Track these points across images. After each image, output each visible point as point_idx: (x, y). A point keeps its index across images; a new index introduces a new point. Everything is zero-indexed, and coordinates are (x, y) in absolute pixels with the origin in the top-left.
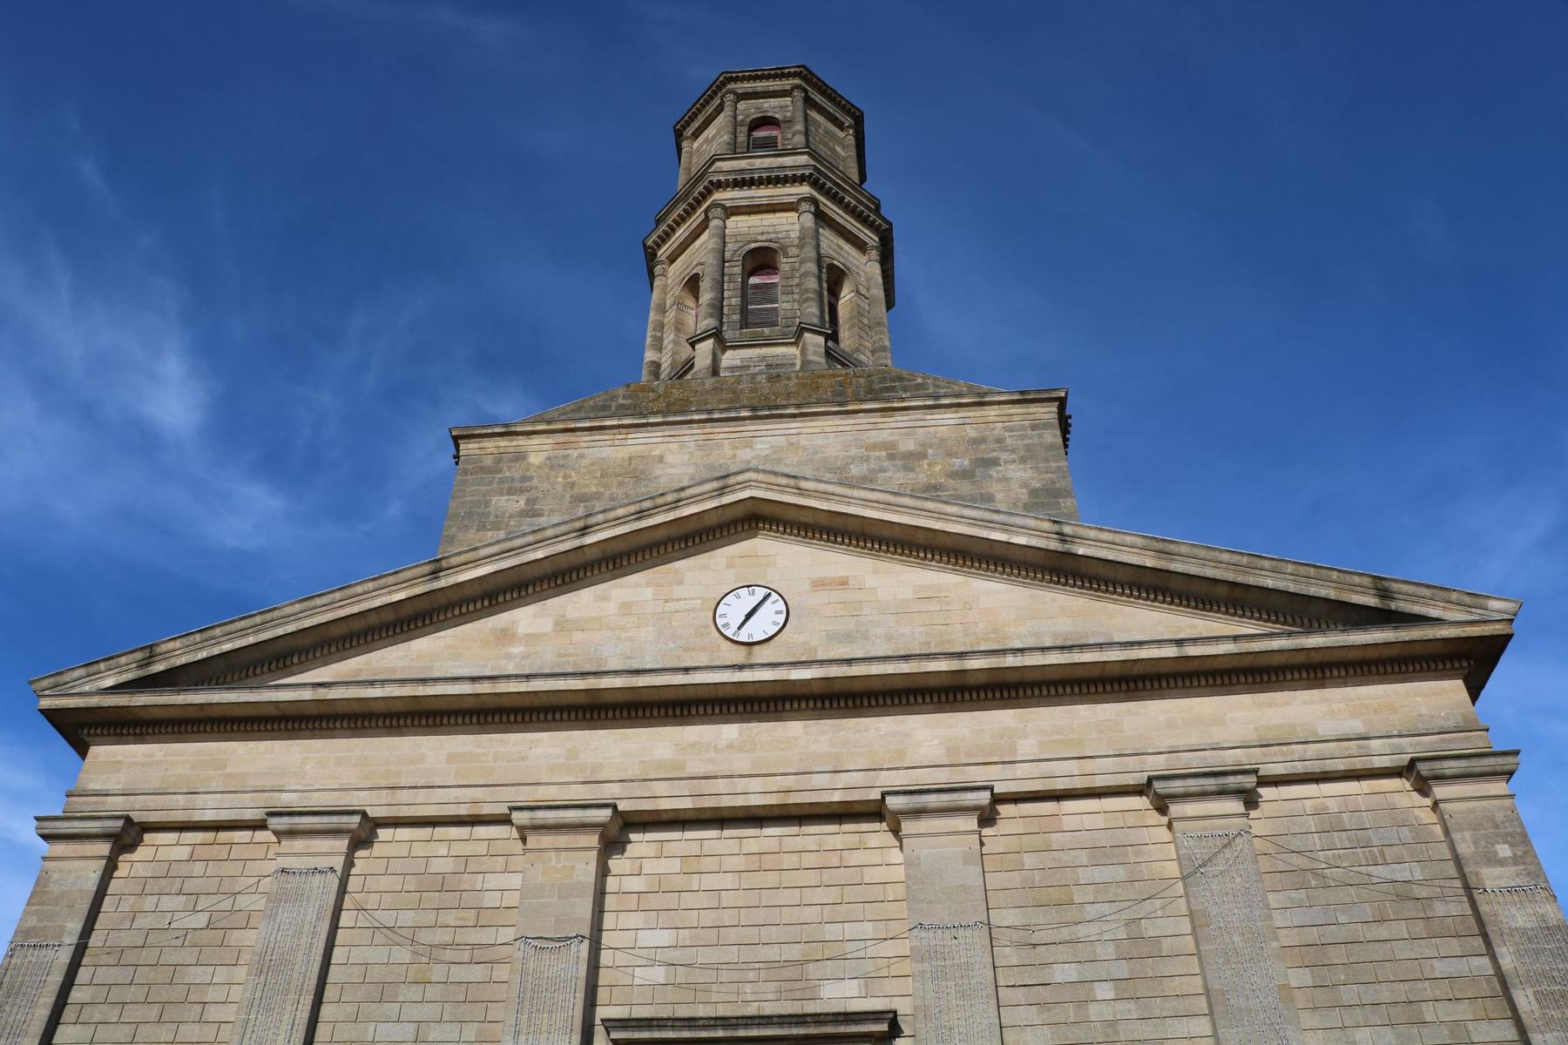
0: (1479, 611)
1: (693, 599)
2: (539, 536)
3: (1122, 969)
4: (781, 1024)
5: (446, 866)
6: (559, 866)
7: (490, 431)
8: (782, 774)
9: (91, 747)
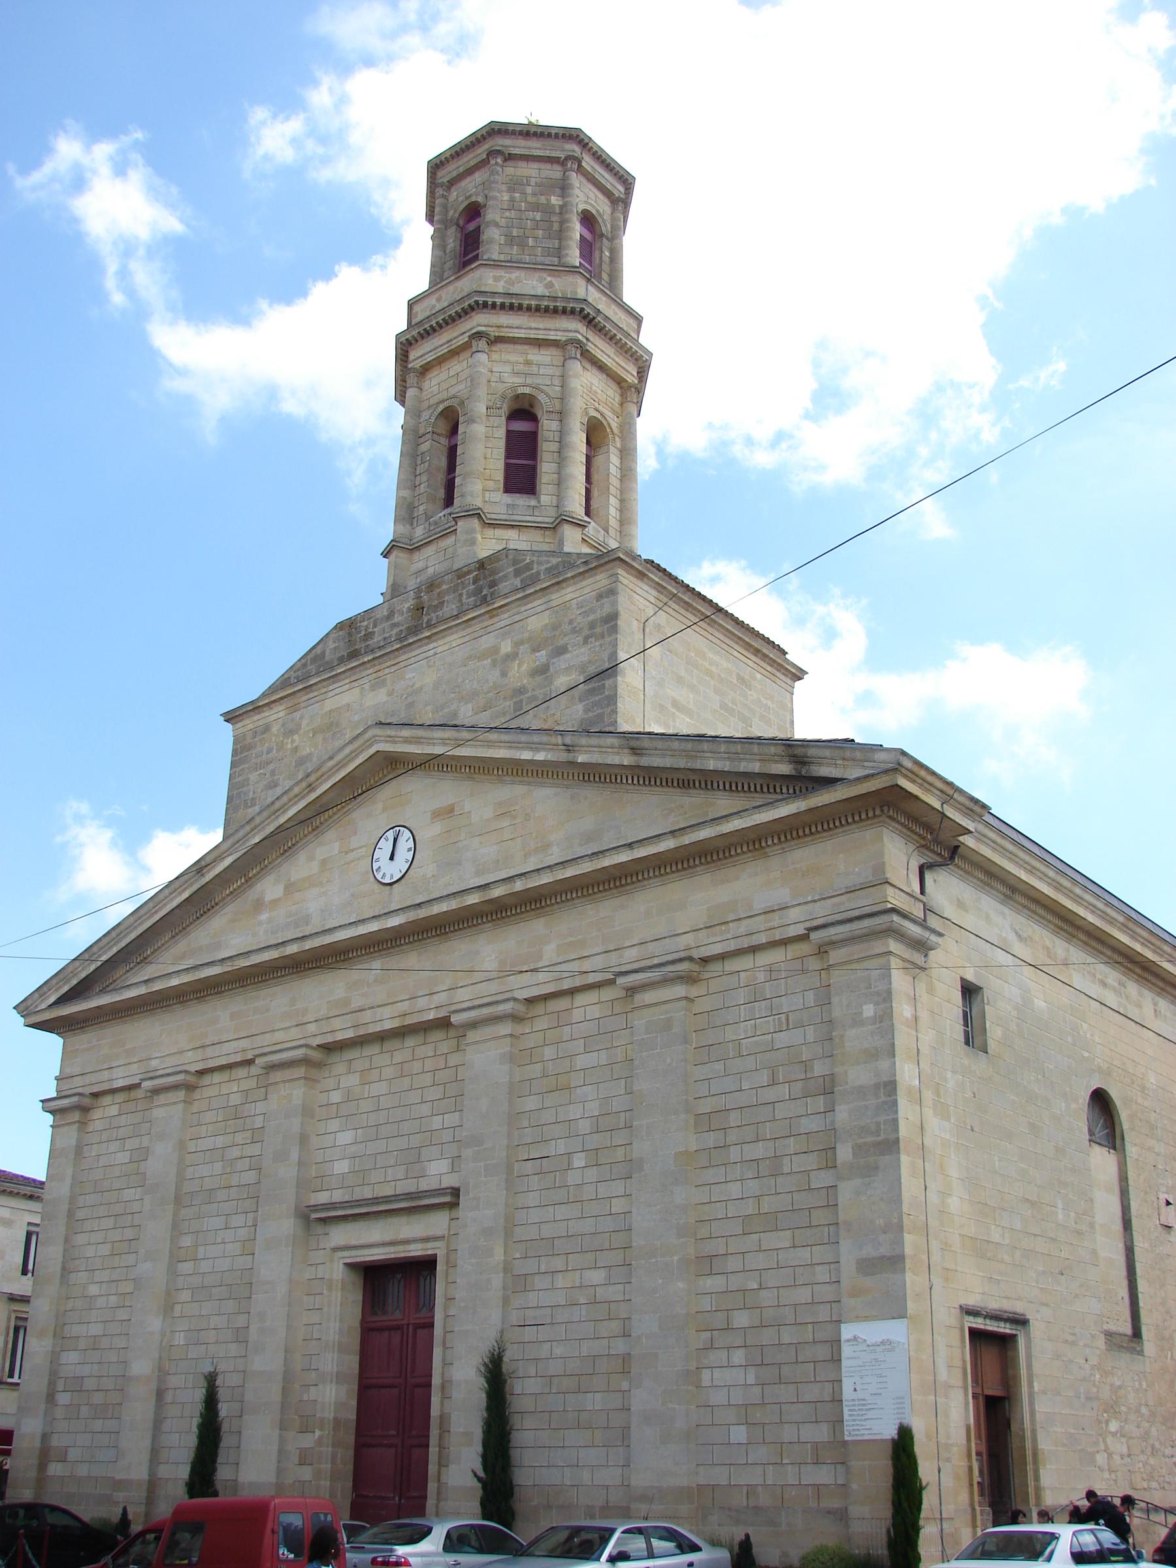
0: (872, 764)
1: (361, 847)
2: (252, 825)
3: (594, 1141)
4: (367, 1205)
5: (235, 1099)
6: (285, 1094)
7: (244, 710)
8: (401, 1001)
9: (61, 1040)
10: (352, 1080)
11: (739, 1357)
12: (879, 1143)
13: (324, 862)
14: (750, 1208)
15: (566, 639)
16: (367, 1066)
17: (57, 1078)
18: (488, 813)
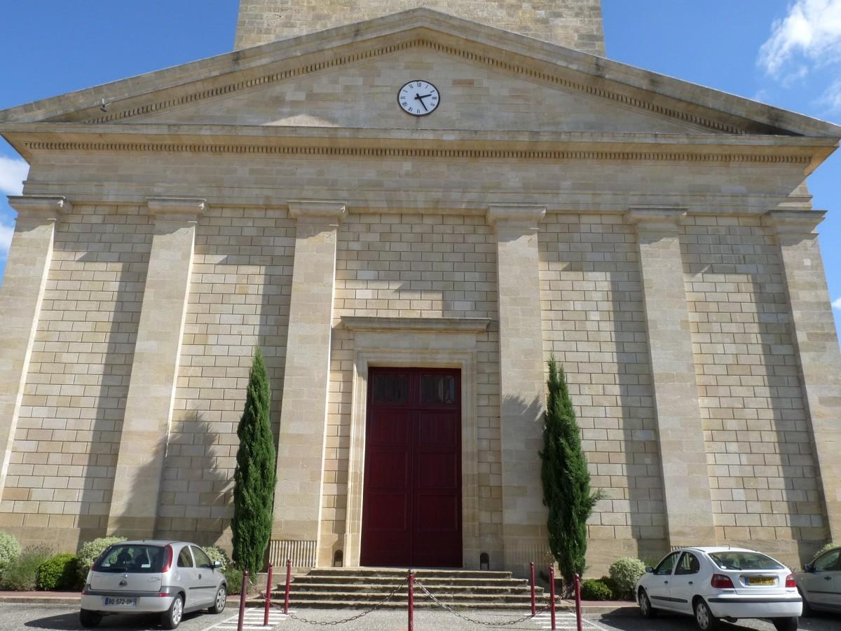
5: (249, 232)
10: (373, 238)
11: (733, 447)
12: (824, 335)
13: (347, 88)
14: (731, 360)
15: (561, 10)
16: (142, 209)
17: (24, 183)
18: (505, 92)
